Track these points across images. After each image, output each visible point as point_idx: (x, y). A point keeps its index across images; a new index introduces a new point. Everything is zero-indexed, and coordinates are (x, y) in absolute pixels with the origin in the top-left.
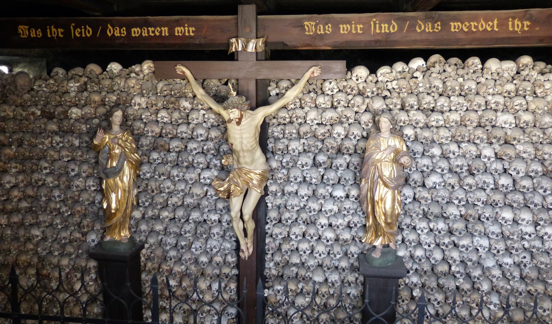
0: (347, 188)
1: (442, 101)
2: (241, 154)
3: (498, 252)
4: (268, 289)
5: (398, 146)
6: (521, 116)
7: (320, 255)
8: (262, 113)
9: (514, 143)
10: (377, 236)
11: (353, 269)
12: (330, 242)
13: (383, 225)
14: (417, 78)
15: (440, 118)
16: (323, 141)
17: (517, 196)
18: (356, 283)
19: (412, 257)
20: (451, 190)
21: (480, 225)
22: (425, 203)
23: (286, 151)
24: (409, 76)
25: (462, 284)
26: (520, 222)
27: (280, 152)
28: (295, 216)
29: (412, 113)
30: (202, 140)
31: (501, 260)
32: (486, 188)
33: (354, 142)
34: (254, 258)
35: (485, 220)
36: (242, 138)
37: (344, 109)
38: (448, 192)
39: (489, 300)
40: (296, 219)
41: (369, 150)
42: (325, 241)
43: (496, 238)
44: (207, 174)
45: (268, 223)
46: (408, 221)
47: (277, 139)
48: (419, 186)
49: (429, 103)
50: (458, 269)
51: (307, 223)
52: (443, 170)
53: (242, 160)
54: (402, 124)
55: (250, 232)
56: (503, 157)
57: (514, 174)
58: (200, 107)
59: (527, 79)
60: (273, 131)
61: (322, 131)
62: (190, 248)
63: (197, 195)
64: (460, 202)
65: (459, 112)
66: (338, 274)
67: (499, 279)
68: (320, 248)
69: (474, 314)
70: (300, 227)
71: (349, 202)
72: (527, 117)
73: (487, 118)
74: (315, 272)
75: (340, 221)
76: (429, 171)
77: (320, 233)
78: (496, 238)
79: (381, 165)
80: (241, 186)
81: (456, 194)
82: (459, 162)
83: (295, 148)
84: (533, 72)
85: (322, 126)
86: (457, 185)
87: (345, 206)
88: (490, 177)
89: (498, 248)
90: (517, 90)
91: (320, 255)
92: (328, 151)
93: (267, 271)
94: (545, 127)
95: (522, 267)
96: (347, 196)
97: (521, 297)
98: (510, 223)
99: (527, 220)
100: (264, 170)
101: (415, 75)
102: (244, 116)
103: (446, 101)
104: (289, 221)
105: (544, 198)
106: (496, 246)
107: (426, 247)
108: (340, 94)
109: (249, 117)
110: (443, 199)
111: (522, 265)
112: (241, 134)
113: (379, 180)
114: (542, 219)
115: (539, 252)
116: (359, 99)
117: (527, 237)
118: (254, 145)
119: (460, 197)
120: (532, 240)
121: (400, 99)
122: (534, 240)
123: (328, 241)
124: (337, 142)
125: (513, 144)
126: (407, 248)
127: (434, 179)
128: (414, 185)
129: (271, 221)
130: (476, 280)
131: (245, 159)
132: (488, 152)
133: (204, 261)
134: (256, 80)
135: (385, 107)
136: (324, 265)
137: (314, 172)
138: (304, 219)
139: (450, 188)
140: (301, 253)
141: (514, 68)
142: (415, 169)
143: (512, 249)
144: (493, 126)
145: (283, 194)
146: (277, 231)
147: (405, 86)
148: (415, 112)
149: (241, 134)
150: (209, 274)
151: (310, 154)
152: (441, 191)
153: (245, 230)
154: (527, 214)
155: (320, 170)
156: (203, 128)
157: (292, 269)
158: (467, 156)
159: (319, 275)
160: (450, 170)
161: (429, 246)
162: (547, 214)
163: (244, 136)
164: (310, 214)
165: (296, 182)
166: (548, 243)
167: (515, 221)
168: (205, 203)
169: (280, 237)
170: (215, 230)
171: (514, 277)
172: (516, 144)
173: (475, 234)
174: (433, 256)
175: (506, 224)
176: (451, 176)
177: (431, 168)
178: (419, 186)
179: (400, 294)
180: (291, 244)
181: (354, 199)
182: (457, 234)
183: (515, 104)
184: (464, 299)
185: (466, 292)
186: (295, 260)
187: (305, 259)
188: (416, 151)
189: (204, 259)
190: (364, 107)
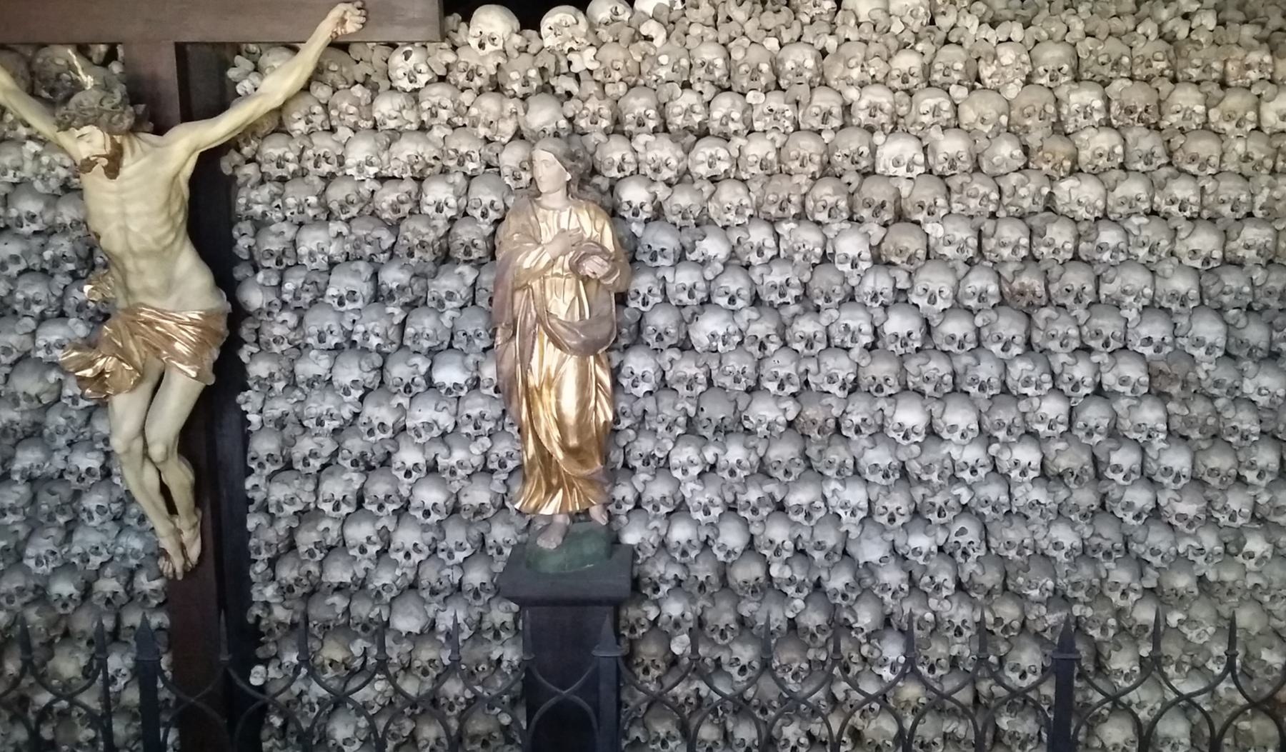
0: (470, 360)
1: (724, 105)
2: (129, 264)
3: (892, 519)
4: (265, 662)
5: (589, 230)
6: (936, 141)
7: (408, 555)
8: (186, 143)
9: (920, 217)
10: (551, 491)
11: (499, 590)
12: (434, 517)
13: (559, 455)
14: (648, 39)
15: (722, 153)
16: (394, 227)
17: (932, 365)
18: (516, 628)
19: (663, 545)
20: (758, 354)
21: (841, 449)
22: (688, 393)
23: (287, 261)
24: (626, 33)
25: (803, 611)
26: (945, 435)
27: (271, 263)
28: (329, 446)
29: (642, 139)
30: (35, 233)
31: (899, 542)
32: (849, 345)
33: (484, 227)
34: (210, 572)
35: (851, 434)
36: (124, 215)
37: (448, 131)
38: (749, 359)
39: (876, 654)
40: (335, 454)
41: (506, 244)
42: (419, 514)
43: (884, 482)
44: (53, 333)
45: (252, 471)
46: (645, 445)
47: (260, 224)
48: (670, 347)
49: (690, 110)
50: (787, 573)
51: (366, 466)
52: (732, 300)
53: (134, 284)
54: (614, 173)
55: (182, 497)
56: (893, 259)
57: (923, 302)
58: (23, 131)
59: (953, 39)
60: (249, 201)
61: (392, 197)
62: (20, 558)
63: (28, 398)
64: (781, 387)
65: (769, 136)
66: (464, 607)
67: (902, 594)
68: (407, 536)
69: (840, 696)
70: (346, 477)
71: (480, 401)
72: (951, 145)
73: (847, 152)
74: (396, 605)
75: (458, 455)
76: (695, 302)
77: (404, 492)
78: (884, 482)
79: (543, 286)
80: (137, 359)
81: (769, 368)
82: (776, 277)
83: (315, 249)
84: (969, 17)
85: (390, 185)
86: (774, 338)
87: (469, 412)
88: (861, 314)
89: (890, 510)
90: (927, 69)
91: (408, 555)
92: (411, 255)
93: (256, 611)
94: (1002, 171)
95: (959, 559)
96: (476, 384)
97: (959, 640)
98: (920, 439)
99: (962, 427)
100: (207, 312)
101: (644, 30)
102: (127, 149)
103: (734, 105)
104: (312, 461)
105: (1005, 365)
106: (887, 504)
107: (699, 516)
108: (438, 89)
109: (145, 153)
110: (737, 381)
111: (959, 552)
112: (122, 203)
113: (539, 328)
114: (1000, 425)
115: (1000, 516)
116: (490, 104)
117: (966, 475)
118: (165, 236)
119: (782, 373)
120: (980, 483)
121: (608, 102)
122: (986, 481)
123: (427, 514)
124: (435, 228)
125: (918, 223)
126: (648, 522)
127: (709, 327)
128: (656, 345)
129: (261, 465)
130: (839, 600)
131: (144, 277)
132: (851, 245)
133: (66, 594)
134: (181, 49)
135: (563, 123)
136: (424, 583)
137: (375, 316)
138: (356, 453)
139: (754, 349)
140: (351, 553)
141: (922, 10)
142: (659, 300)
143: (929, 512)
144: (865, 174)
145: (293, 384)
146: (279, 492)
147: (620, 65)
148: (651, 138)
149: (122, 203)
150: (83, 632)
151: (362, 266)
152: (732, 357)
153: (165, 490)
154: (962, 411)
155: (390, 310)
156: (37, 195)
157: (330, 601)
158: (798, 257)
159: (411, 614)
160: (756, 301)
161: (707, 513)
162: (1014, 409)
163: (132, 209)
164: (372, 439)
165: (323, 346)
166: (1022, 488)
167: (932, 432)
168: (56, 419)
169: (290, 510)
170: (92, 501)
171: (938, 588)
172: (926, 222)
173: (828, 473)
174: (720, 541)
175: (905, 442)
176: (754, 315)
177: (700, 295)
178: (670, 347)
179: (640, 652)
180: (321, 527)
181: (492, 389)
182: (779, 474)
183: (923, 109)
184: (811, 654)
185: (813, 635)
186: (338, 573)
187: (367, 570)
188: (656, 248)
189: (64, 587)
190: (508, 128)
